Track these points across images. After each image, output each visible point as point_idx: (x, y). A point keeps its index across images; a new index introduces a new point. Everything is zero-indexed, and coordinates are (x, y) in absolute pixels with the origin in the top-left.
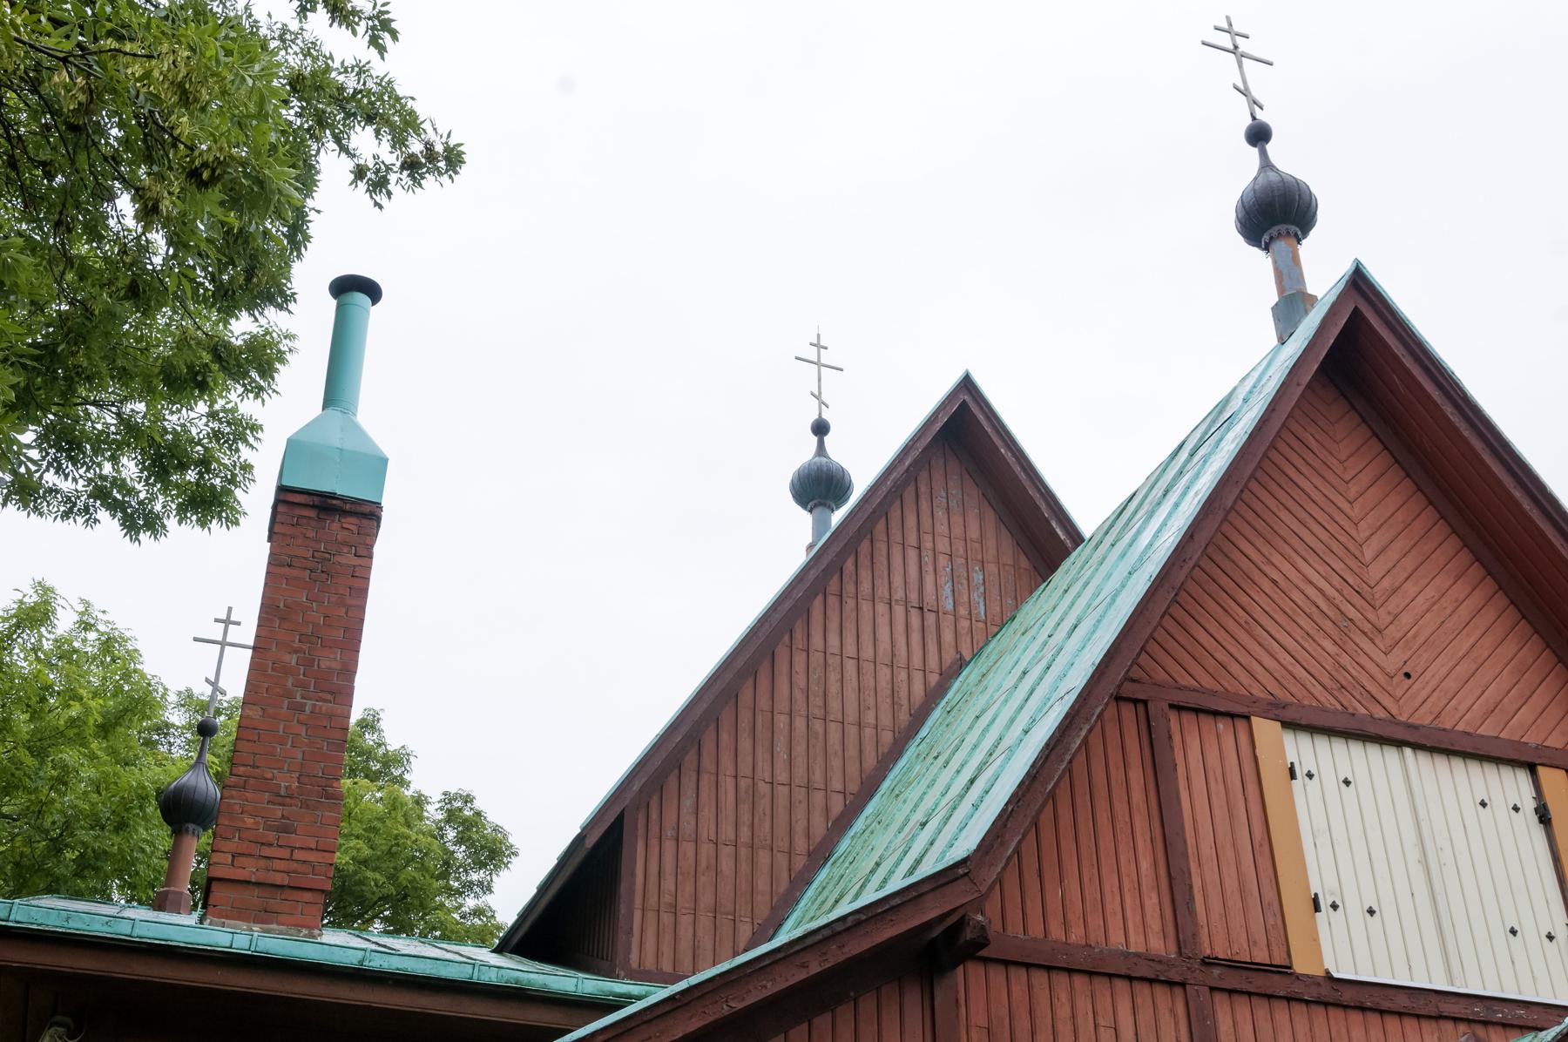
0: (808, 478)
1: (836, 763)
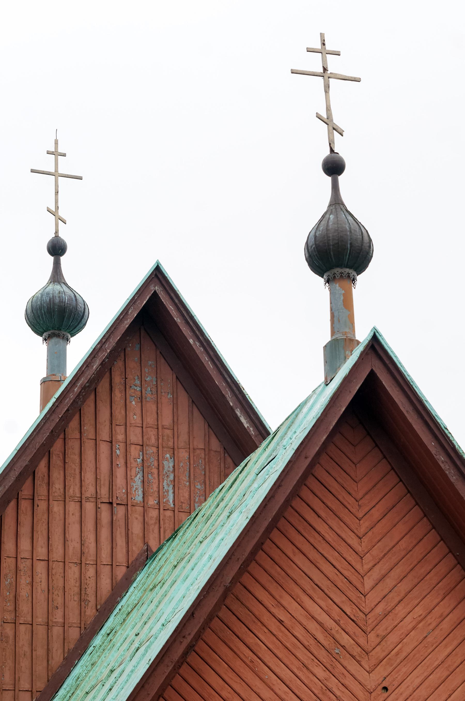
0: (41, 310)
1: (24, 664)
